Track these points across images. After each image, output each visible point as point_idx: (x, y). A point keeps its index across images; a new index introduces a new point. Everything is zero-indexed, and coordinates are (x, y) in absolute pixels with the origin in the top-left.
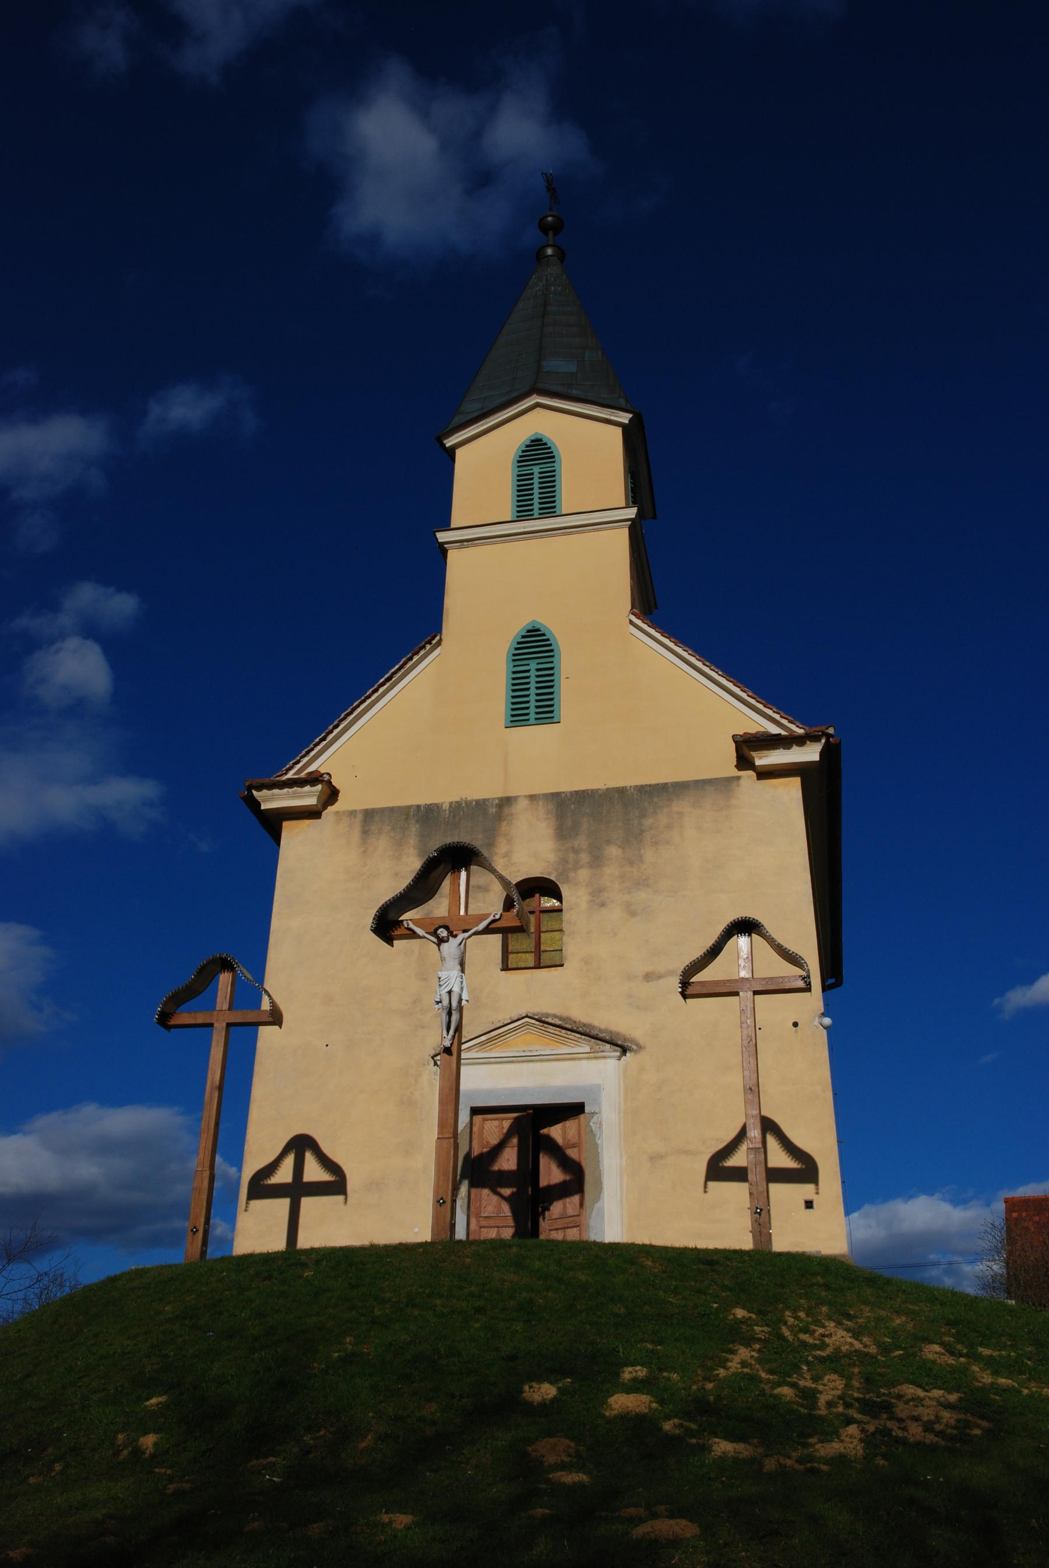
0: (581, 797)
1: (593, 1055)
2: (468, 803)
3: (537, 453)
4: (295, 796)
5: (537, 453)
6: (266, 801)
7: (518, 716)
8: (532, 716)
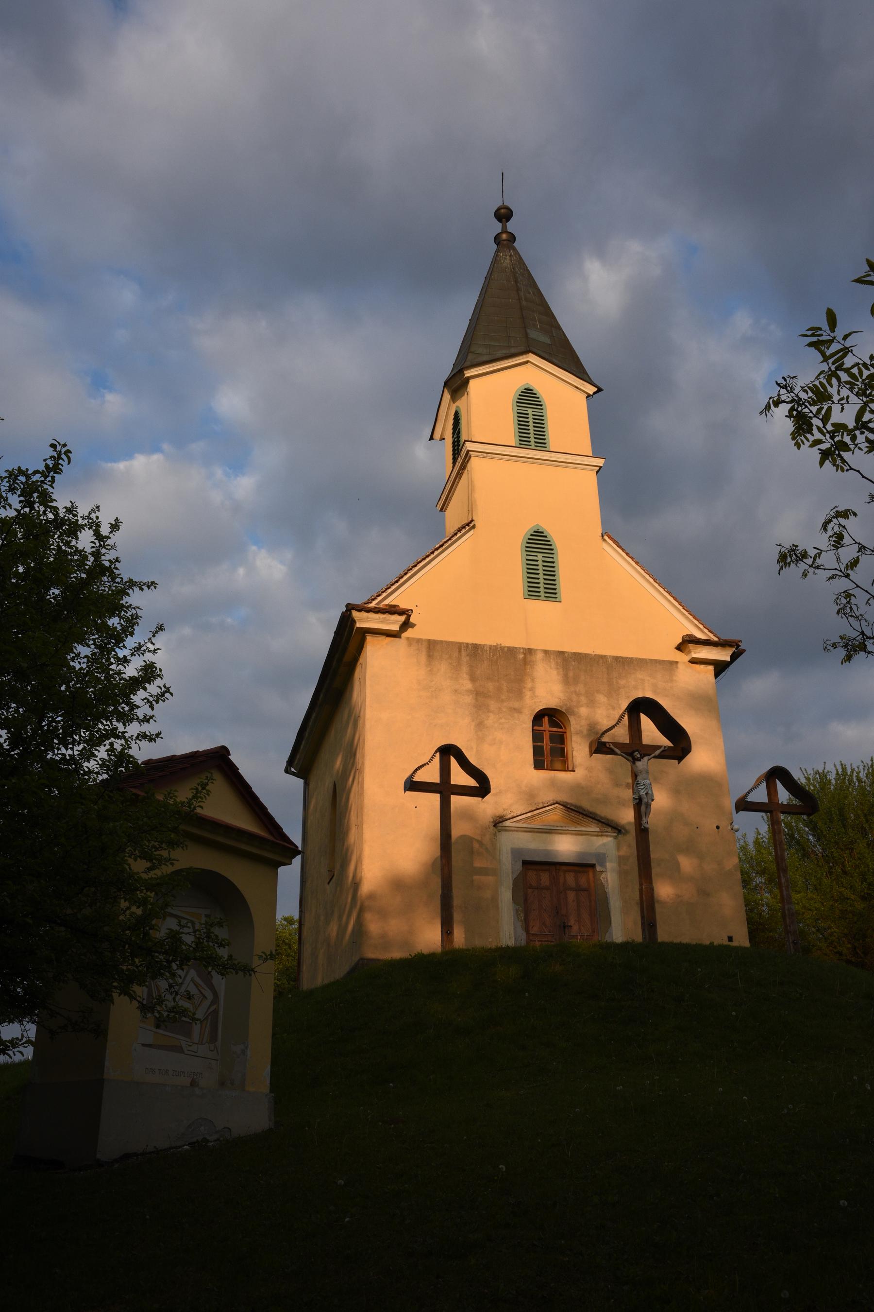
0: (579, 657)
1: (600, 834)
2: (502, 648)
3: (528, 398)
4: (384, 621)
5: (528, 398)
6: (361, 621)
7: (532, 592)
8: (542, 594)
